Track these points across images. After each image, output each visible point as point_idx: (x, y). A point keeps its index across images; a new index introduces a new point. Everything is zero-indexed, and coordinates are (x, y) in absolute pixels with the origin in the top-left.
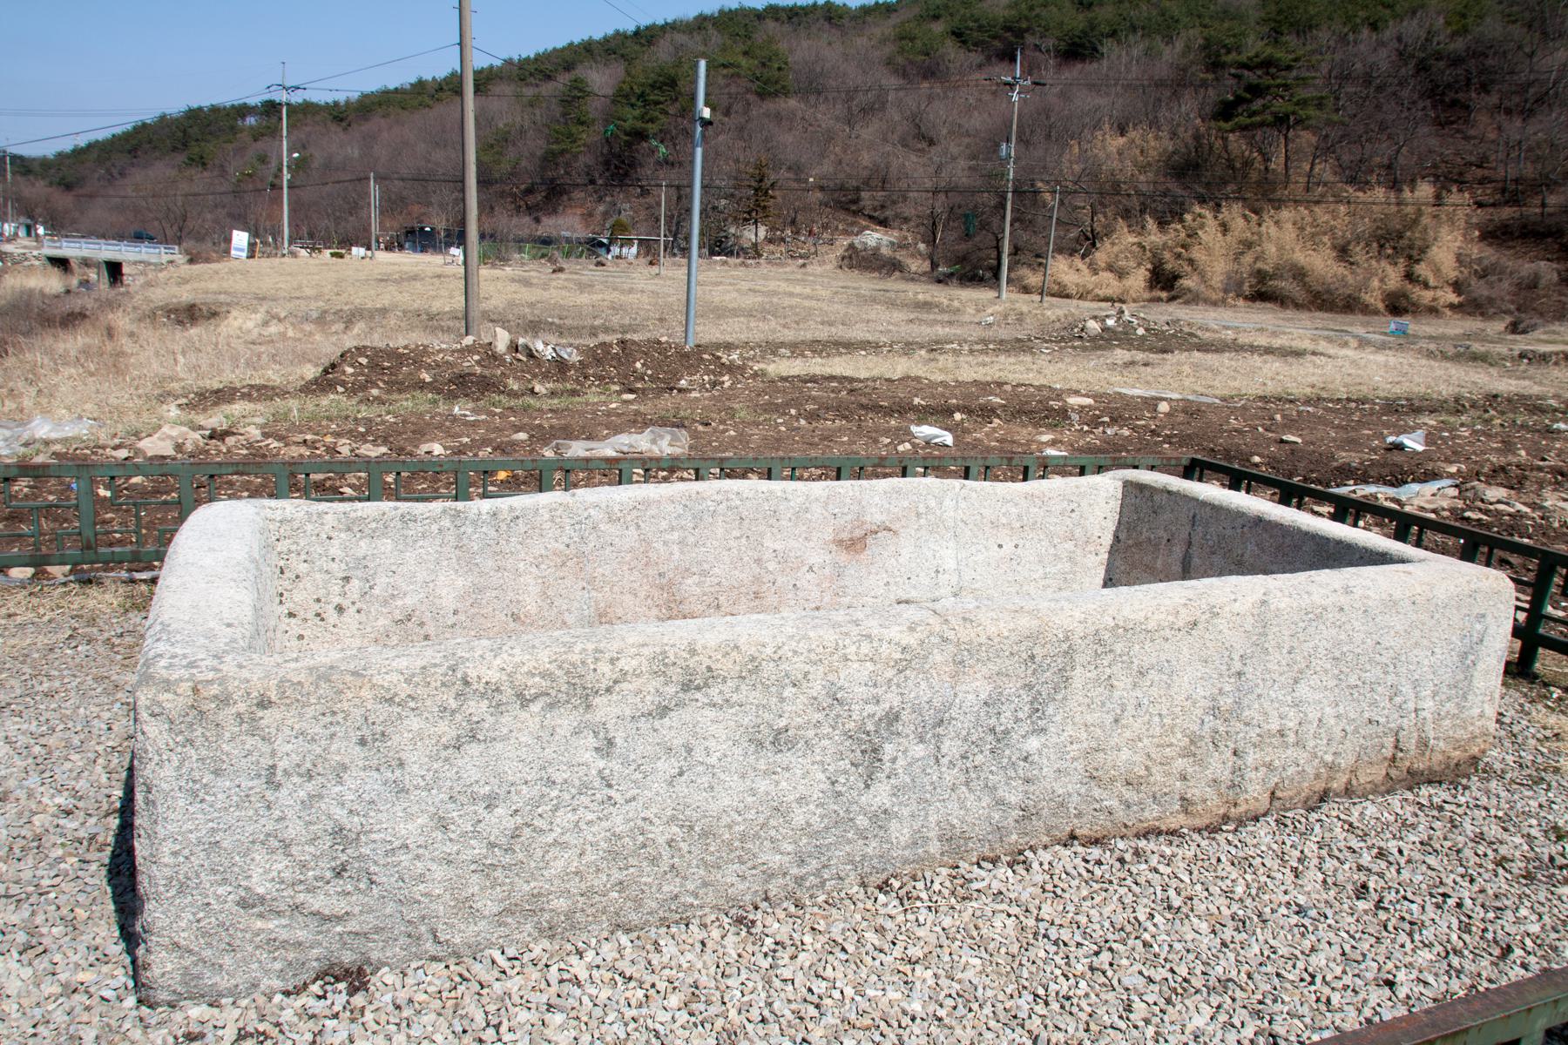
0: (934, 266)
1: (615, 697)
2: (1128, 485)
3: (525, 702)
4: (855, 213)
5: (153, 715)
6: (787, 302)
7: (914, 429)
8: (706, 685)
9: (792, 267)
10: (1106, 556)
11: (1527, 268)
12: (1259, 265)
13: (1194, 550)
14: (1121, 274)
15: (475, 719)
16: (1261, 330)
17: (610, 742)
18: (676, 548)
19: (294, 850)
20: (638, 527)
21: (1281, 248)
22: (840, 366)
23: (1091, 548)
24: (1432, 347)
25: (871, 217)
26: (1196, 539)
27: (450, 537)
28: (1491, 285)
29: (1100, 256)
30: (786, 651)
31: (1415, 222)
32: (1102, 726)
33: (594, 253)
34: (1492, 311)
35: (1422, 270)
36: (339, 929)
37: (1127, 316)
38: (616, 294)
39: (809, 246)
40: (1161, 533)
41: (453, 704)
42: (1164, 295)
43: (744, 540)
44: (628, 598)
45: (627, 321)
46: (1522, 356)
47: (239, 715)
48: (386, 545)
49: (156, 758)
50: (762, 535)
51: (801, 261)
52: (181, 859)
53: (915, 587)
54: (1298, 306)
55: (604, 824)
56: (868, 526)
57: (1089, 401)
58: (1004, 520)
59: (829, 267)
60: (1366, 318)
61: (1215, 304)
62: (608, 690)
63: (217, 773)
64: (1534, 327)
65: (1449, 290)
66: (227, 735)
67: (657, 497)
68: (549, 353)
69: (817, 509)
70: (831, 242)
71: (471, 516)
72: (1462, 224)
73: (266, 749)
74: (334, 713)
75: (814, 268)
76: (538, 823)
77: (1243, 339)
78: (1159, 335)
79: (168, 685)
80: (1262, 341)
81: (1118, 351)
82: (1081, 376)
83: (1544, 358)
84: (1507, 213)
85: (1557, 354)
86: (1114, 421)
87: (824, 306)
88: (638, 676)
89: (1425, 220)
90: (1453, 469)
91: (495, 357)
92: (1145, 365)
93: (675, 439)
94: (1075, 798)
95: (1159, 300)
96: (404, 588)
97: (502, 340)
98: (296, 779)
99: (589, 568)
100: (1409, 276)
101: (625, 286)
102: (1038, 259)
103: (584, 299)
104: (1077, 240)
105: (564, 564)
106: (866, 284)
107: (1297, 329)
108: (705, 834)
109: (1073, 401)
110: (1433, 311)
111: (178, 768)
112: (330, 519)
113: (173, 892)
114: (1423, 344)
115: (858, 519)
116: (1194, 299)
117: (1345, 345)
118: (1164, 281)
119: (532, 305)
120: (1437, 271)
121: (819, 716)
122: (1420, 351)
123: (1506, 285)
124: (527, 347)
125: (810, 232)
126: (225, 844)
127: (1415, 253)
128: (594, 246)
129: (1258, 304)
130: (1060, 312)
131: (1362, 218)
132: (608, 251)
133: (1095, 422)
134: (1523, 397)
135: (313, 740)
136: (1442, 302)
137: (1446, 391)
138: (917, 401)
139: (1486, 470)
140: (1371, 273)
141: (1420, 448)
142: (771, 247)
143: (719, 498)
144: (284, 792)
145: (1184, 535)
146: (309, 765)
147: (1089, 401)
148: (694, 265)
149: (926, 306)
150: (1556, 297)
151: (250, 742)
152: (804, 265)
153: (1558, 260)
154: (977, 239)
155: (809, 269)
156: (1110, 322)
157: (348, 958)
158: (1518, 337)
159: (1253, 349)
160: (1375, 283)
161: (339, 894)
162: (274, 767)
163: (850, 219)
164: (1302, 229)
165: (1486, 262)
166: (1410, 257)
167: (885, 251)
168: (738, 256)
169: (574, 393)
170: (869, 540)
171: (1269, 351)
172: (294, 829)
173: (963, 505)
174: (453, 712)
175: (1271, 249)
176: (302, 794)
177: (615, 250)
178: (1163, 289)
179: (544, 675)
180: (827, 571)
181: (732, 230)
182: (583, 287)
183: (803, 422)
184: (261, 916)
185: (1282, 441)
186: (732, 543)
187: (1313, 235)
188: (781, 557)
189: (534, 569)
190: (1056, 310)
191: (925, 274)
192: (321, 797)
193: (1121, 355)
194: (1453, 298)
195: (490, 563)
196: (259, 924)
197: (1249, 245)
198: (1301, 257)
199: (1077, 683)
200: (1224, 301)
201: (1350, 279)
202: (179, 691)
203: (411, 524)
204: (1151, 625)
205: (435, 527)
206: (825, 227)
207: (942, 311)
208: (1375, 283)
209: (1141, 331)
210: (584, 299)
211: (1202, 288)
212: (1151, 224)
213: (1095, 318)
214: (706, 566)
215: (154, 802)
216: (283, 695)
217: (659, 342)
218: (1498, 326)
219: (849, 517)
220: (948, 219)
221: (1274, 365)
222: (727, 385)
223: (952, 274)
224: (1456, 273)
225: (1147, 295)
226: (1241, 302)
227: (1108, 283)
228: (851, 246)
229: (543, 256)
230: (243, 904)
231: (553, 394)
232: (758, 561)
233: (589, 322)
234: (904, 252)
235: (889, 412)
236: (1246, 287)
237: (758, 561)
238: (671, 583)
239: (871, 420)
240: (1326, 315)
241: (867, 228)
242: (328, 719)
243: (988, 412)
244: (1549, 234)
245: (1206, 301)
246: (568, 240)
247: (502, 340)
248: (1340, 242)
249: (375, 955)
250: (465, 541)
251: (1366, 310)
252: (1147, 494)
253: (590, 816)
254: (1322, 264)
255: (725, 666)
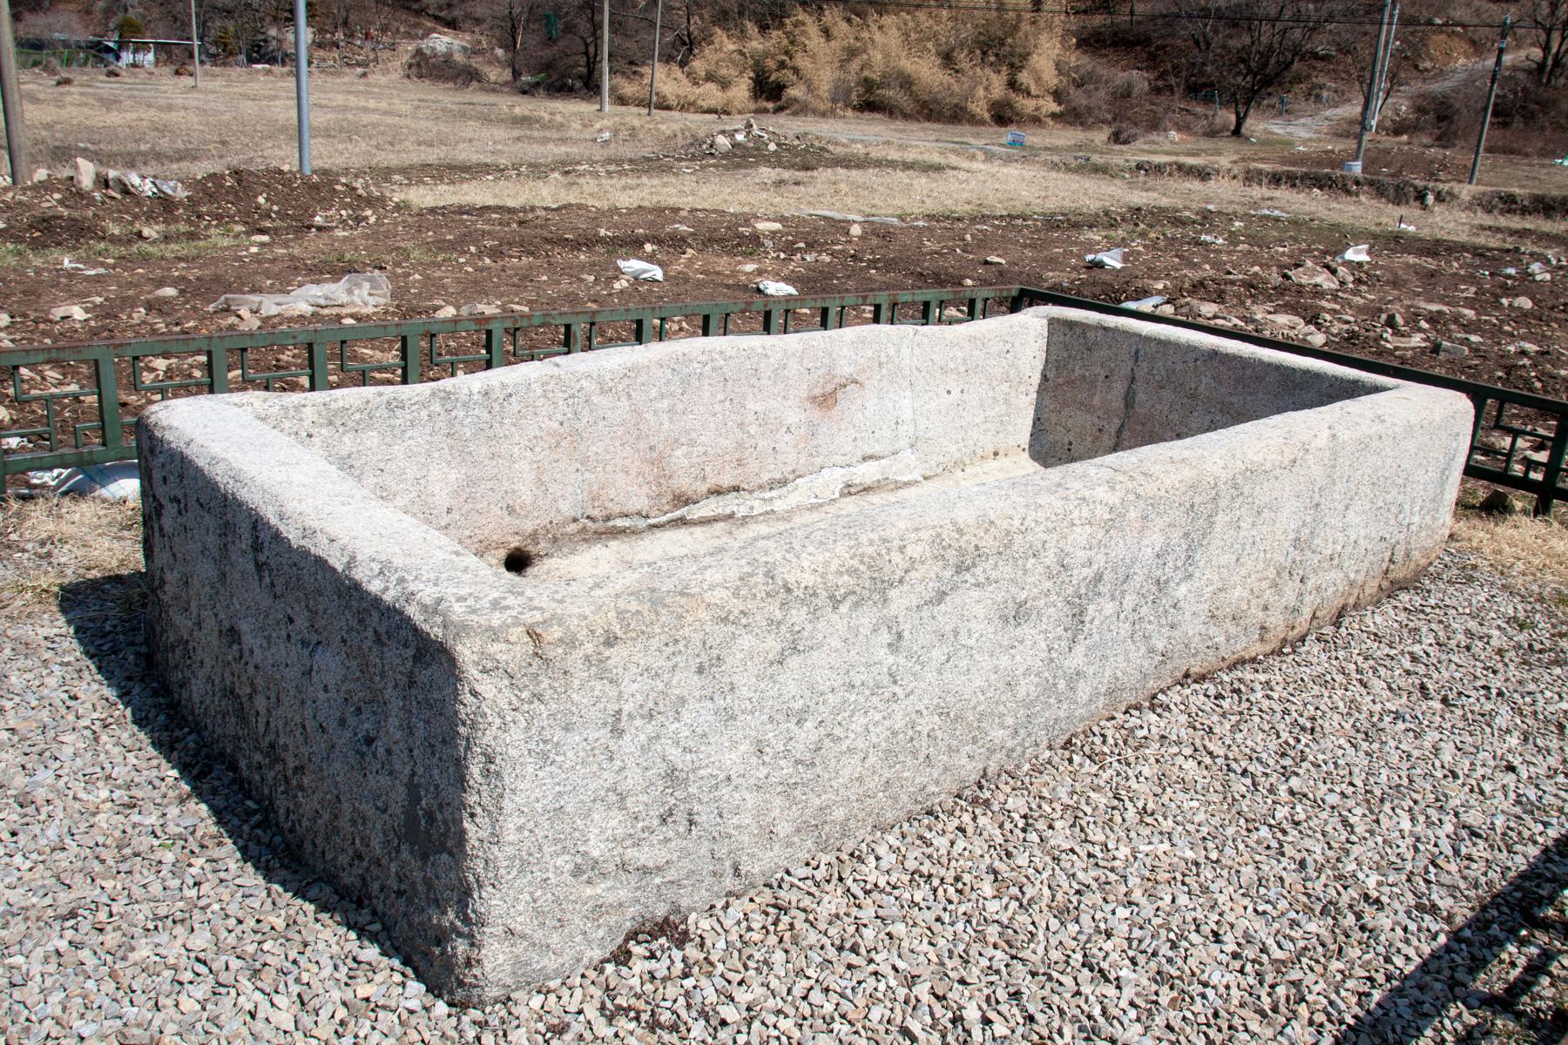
0: (516, 74)
1: (906, 588)
2: (1053, 322)
3: (835, 602)
4: (418, 13)
5: (485, 671)
6: (367, 119)
7: (621, 264)
8: (974, 565)
9: (350, 76)
10: (1035, 396)
11: (1121, 77)
12: (866, 73)
13: (1139, 386)
14: (724, 84)
15: (797, 628)
16: (888, 143)
17: (900, 636)
18: (665, 417)
19: (629, 802)
20: (629, 396)
21: (887, 56)
22: (476, 193)
23: (1022, 389)
24: (1056, 159)
25: (436, 18)
26: (1140, 374)
27: (441, 423)
28: (1088, 94)
29: (698, 65)
30: (1029, 522)
31: (1016, 28)
32: (1227, 567)
33: (102, 60)
34: (1091, 120)
35: (1024, 78)
36: (658, 880)
37: (756, 131)
38: (152, 112)
39: (366, 52)
40: (1098, 370)
41: (779, 615)
42: (770, 105)
43: (727, 403)
44: (620, 477)
45: (180, 145)
46: (1139, 167)
47: (587, 658)
48: (372, 438)
49: (498, 721)
50: (744, 396)
51: (359, 70)
52: (527, 833)
53: (878, 441)
54: (906, 116)
55: (887, 723)
56: (837, 380)
57: (777, 226)
58: (952, 366)
59: (395, 76)
60: (975, 129)
61: (823, 115)
62: (901, 581)
63: (567, 728)
64: (1134, 137)
65: (1050, 98)
66: (577, 682)
67: (646, 362)
68: (148, 188)
69: (794, 365)
70: (393, 47)
71: (463, 397)
72: (1059, 31)
73: (612, 692)
74: (676, 641)
75: (377, 78)
76: (838, 731)
77: (875, 154)
78: (791, 149)
79: (494, 634)
80: (894, 155)
81: (763, 169)
82: (743, 197)
83: (1159, 169)
84: (1098, 20)
85: (1170, 165)
86: (810, 246)
87: (408, 122)
88: (923, 563)
89: (1025, 27)
90: (1160, 286)
91: (81, 194)
92: (797, 183)
93: (375, 285)
94: (1197, 638)
95: (766, 111)
96: (394, 487)
97: (86, 173)
98: (638, 722)
99: (582, 448)
100: (1012, 85)
101: (162, 102)
102: (629, 64)
103: (114, 118)
104: (673, 45)
105: (558, 445)
106: (445, 96)
107: (923, 141)
108: (958, 718)
109: (763, 226)
110: (1036, 120)
111: (527, 729)
112: (308, 412)
113: (514, 873)
114: (1044, 156)
115: (829, 373)
116: (802, 109)
117: (973, 158)
118: (769, 91)
119: (48, 127)
120: (1038, 79)
121: (1049, 584)
122: (1045, 163)
123: (1102, 93)
124: (120, 181)
125: (367, 36)
126: (568, 809)
127: (1016, 60)
128: (99, 53)
129: (867, 115)
130: (676, 127)
131: (964, 23)
132: (118, 58)
133: (790, 249)
134: (1162, 210)
135: (657, 675)
136: (1044, 111)
137: (1092, 205)
138: (602, 232)
139: (1186, 285)
140: (976, 83)
141: (1119, 266)
142: (322, 53)
143: (703, 358)
144: (627, 737)
145: (1125, 369)
146: (651, 704)
147: (777, 226)
148: (304, 77)
149: (524, 121)
150: (1148, 107)
151: (598, 685)
152: (364, 75)
153: (1147, 69)
154: (561, 43)
155: (371, 78)
156: (740, 137)
157: (661, 911)
158: (1124, 147)
159: (892, 164)
160: (981, 92)
161: (660, 842)
162: (619, 712)
163: (413, 20)
164: (907, 35)
165: (1082, 71)
166: (1012, 65)
167: (459, 58)
168: (284, 64)
169: (192, 236)
170: (840, 395)
171: (907, 166)
172: (633, 779)
173: (917, 351)
174: (779, 623)
175: (877, 57)
176: (643, 737)
177: (127, 57)
178: (768, 99)
179: (853, 572)
180: (802, 431)
181: (273, 32)
182: (109, 104)
183: (487, 261)
184: (589, 882)
185: (986, 263)
186: (718, 408)
187: (919, 40)
188: (762, 419)
189: (528, 454)
190: (671, 123)
191: (506, 83)
192: (658, 737)
193: (767, 173)
194: (1054, 107)
195: (484, 450)
196: (589, 891)
197: (852, 53)
198: (907, 65)
199: (1218, 528)
200: (832, 111)
201: (956, 88)
202: (513, 639)
203: (398, 412)
204: (1268, 466)
205: (424, 413)
206: (384, 29)
207: (544, 127)
208: (981, 92)
209: (772, 147)
210: (114, 118)
211: (810, 98)
212: (751, 28)
213: (723, 132)
214: (694, 435)
215: (498, 774)
216: (627, 628)
217: (281, 172)
218: (1100, 136)
219: (821, 372)
220: (528, 21)
221: (921, 182)
222: (372, 220)
223: (538, 84)
224: (1056, 81)
225: (753, 106)
226: (849, 113)
227: (711, 94)
228: (419, 52)
229: (36, 64)
230: (577, 871)
231: (167, 238)
232: (741, 425)
233: (131, 147)
234: (480, 59)
235: (576, 246)
236: (854, 96)
237: (741, 425)
238: (661, 457)
239: (560, 256)
240: (935, 126)
241: (433, 30)
242: (670, 650)
243: (677, 243)
244: (1138, 43)
245: (814, 112)
246: (66, 44)
247: (86, 173)
248: (944, 48)
249: (685, 903)
250: (458, 427)
251: (973, 120)
252: (1078, 331)
253: (878, 717)
254: (928, 72)
255: (989, 543)
